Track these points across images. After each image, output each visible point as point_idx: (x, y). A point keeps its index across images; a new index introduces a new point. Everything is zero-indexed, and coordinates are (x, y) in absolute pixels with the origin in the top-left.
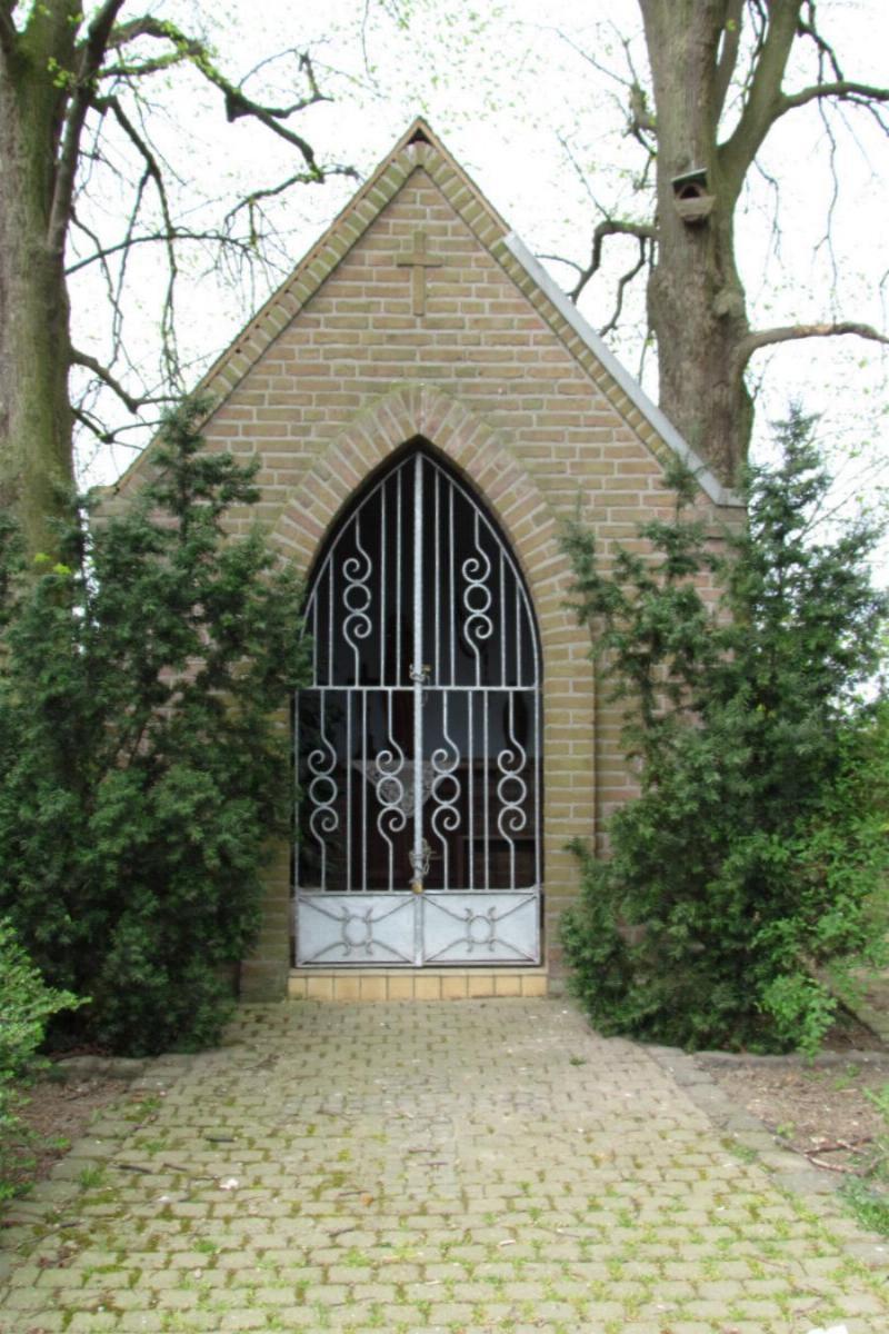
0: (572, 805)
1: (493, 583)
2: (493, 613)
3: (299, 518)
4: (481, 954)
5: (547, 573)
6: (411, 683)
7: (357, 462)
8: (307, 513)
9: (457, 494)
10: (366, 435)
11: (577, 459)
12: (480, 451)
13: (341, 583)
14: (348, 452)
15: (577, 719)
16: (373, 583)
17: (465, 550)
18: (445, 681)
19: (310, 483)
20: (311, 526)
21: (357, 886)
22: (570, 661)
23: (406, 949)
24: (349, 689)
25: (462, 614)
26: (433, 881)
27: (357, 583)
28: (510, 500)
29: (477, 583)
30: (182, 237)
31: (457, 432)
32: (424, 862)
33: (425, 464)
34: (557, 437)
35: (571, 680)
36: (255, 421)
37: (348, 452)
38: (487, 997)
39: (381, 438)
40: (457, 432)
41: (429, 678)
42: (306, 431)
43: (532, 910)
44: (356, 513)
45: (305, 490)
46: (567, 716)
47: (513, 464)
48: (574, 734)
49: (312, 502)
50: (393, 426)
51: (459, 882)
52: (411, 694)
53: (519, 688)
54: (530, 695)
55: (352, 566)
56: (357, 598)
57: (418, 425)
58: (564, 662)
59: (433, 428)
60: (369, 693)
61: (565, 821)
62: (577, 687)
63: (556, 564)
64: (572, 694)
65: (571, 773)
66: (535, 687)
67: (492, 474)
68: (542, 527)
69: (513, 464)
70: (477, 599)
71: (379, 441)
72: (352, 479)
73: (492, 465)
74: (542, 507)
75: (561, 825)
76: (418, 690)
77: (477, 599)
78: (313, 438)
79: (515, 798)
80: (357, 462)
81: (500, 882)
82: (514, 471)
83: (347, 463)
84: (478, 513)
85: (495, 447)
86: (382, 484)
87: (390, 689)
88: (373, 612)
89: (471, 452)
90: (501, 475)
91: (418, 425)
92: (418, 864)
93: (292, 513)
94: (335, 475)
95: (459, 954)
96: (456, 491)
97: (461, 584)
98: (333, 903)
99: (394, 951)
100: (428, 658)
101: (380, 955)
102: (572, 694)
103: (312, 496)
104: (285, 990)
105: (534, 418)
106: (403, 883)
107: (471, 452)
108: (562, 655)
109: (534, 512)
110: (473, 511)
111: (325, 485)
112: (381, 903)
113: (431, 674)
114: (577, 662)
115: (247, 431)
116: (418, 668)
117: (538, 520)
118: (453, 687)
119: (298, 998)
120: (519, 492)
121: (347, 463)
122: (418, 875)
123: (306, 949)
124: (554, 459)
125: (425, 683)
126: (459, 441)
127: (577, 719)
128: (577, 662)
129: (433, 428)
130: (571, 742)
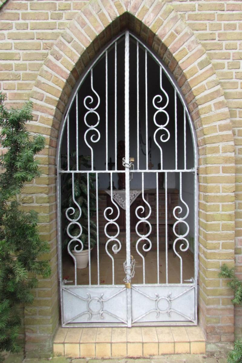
0: (221, 242)
1: (170, 109)
2: (171, 127)
3: (53, 67)
4: (164, 318)
5: (207, 99)
6: (124, 168)
7: (88, 30)
8: (58, 63)
9: (150, 57)
10: (94, 13)
11: (222, 31)
12: (165, 22)
13: (83, 111)
14: (83, 24)
15: (225, 190)
16: (101, 110)
17: (154, 90)
18: (143, 167)
19: (60, 45)
20: (60, 72)
21: (94, 282)
22: (221, 154)
23: (122, 315)
24: (88, 172)
25: (152, 128)
26: (137, 279)
27: (92, 110)
28: (184, 53)
29: (161, 110)
30: (173, 300)
31: (151, 10)
32: (131, 270)
33: (132, 40)
34: (210, 18)
35: (221, 166)
36: (29, 11)
37: (83, 24)
38: (171, 354)
39: (104, 15)
40: (151, 10)
41: (134, 166)
42: (59, 17)
43: (192, 295)
44: (90, 69)
45: (57, 49)
46: (219, 188)
47: (187, 30)
48: (223, 199)
49: (61, 56)
50: (111, 7)
51: (151, 280)
52: (124, 174)
53: (185, 170)
54: (192, 174)
55: (89, 100)
56: (92, 119)
57: (127, 6)
58: (217, 155)
59: (136, 8)
60: (168, 173)
61: (216, 251)
62: (225, 170)
63: (212, 93)
64: (221, 174)
65: (221, 223)
66: (195, 170)
67: (172, 36)
68: (204, 70)
69: (187, 30)
70: (161, 118)
71: (102, 16)
72: (85, 41)
73: (173, 31)
74: (204, 57)
75: (215, 253)
76: (127, 172)
77: (161, 118)
78: (63, 21)
79: (182, 234)
80: (88, 30)
81: (174, 280)
82: (186, 34)
83: (83, 31)
84: (162, 67)
85: (175, 19)
86: (106, 51)
87: (92, 171)
88: (101, 128)
89: (160, 23)
90: (179, 37)
91: (127, 6)
92: (128, 272)
93: (49, 64)
94: (75, 39)
95: (152, 318)
96: (148, 52)
97: (152, 110)
98: (82, 291)
99: (116, 317)
100: (133, 154)
101: (108, 319)
102: (221, 174)
103: (61, 53)
104: (52, 350)
105: (197, 6)
106: (120, 280)
107: (160, 23)
108: (215, 150)
109: (199, 60)
110: (158, 67)
111: (69, 46)
112: (108, 291)
113: (135, 163)
114: (225, 155)
115: (25, 17)
116: (127, 159)
117: (202, 65)
118: (147, 171)
119: (59, 355)
120: (189, 47)
121: (83, 31)
122: (128, 277)
123: (68, 315)
124: (208, 31)
125: (131, 168)
126: (152, 16)
127: (225, 190)
128: (225, 155)
129: (136, 8)
130: (220, 204)
